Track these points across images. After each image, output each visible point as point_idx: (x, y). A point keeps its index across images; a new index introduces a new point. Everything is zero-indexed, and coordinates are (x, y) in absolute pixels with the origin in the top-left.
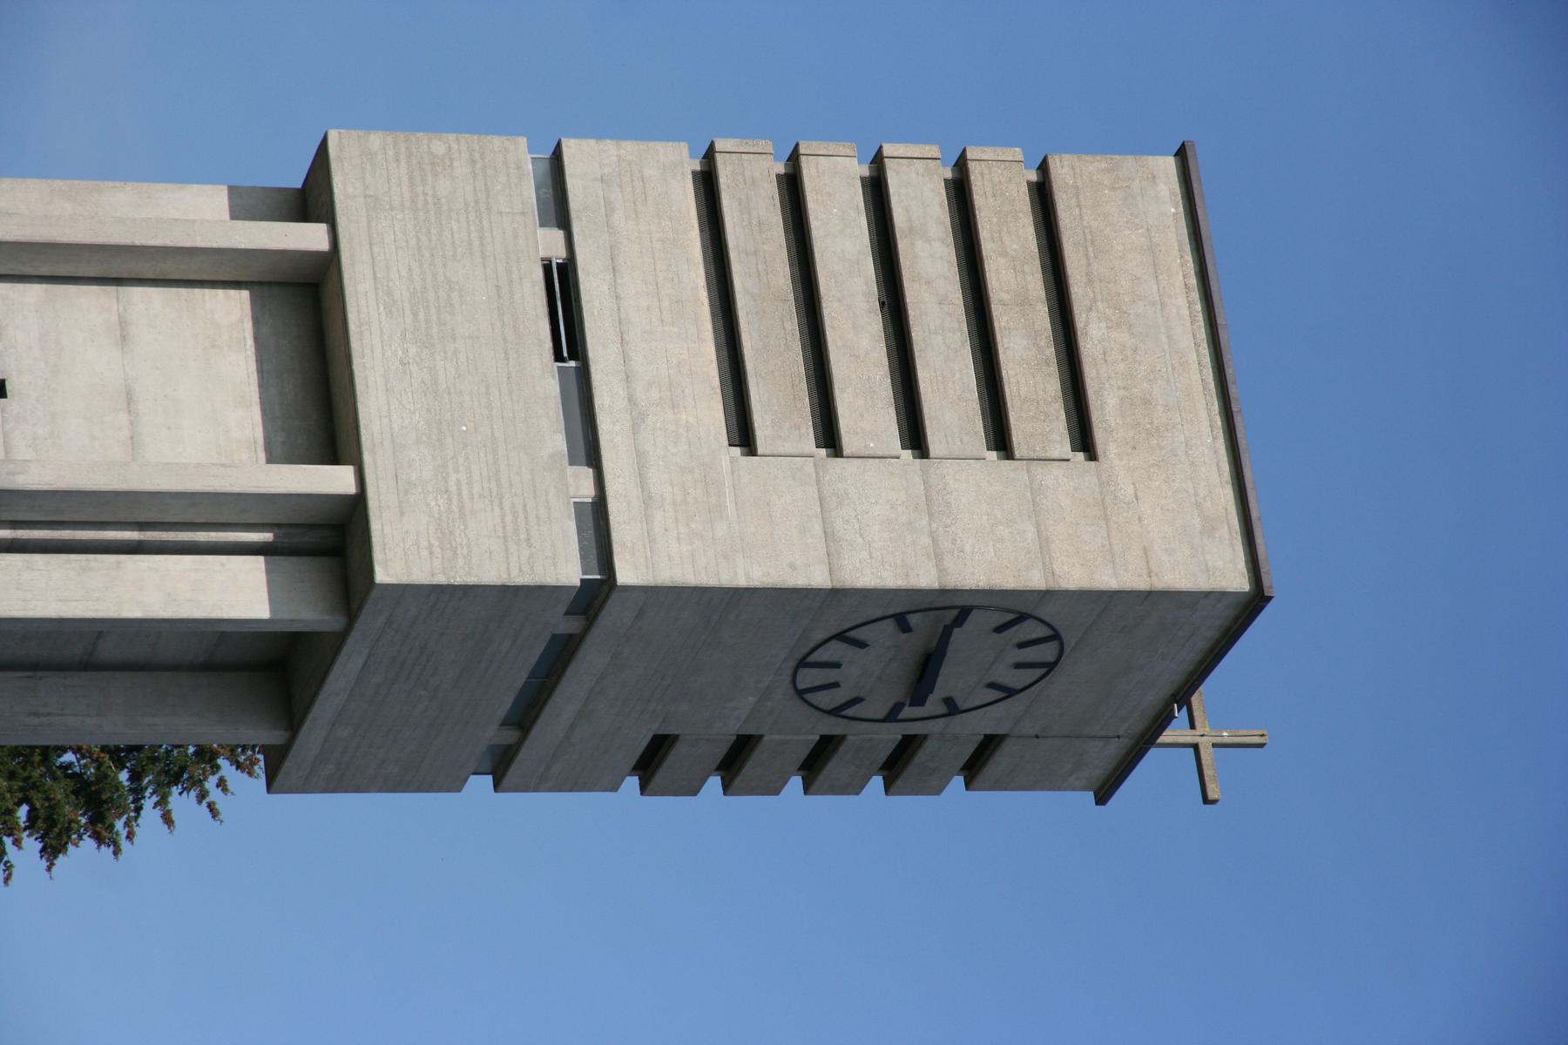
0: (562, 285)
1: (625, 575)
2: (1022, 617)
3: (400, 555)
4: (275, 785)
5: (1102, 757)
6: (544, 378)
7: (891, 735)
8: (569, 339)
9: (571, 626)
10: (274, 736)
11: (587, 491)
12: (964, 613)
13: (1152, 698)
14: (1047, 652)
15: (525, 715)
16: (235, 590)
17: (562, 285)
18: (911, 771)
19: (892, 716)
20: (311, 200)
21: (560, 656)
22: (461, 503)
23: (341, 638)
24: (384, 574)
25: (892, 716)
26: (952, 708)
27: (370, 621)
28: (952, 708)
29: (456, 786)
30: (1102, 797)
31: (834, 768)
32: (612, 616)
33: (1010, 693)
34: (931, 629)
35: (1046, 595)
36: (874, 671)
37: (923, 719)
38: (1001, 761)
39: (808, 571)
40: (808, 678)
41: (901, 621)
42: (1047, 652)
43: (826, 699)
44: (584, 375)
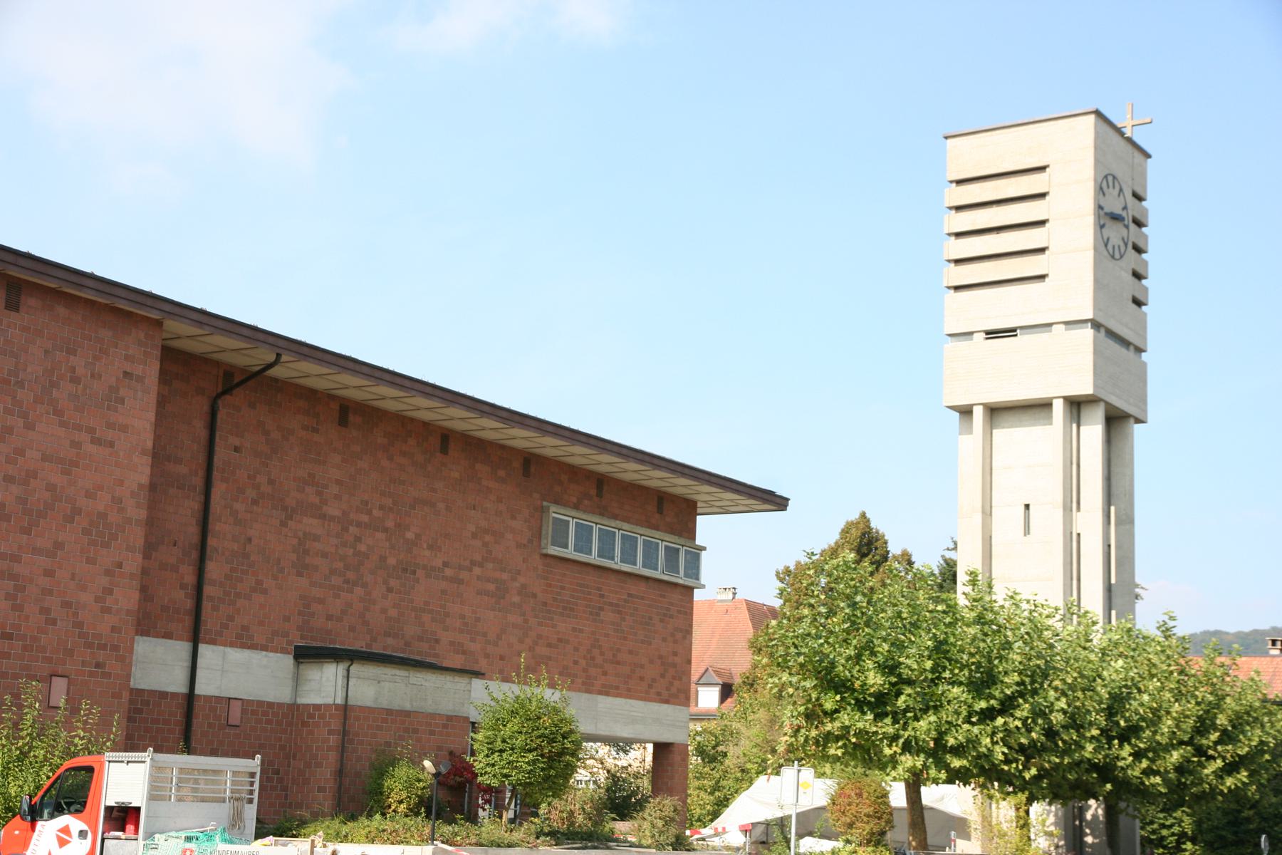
0: (992, 334)
1: (1091, 317)
2: (1101, 188)
3: (1085, 387)
4: (1140, 417)
5: (1138, 157)
6: (1022, 338)
7: (1132, 226)
8: (1010, 332)
9: (1103, 330)
10: (1132, 420)
11: (1063, 326)
12: (1100, 207)
13: (1123, 143)
14: (1110, 178)
17: (992, 334)
18: (1142, 220)
19: (1127, 227)
20: (966, 412)
21: (1111, 334)
22: (1070, 366)
23: (1107, 403)
24: (1090, 391)
25: (1127, 227)
26: (1125, 208)
28: (1125, 208)
30: (1149, 156)
32: (1101, 320)
33: (1121, 190)
34: (1107, 218)
35: (1095, 180)
36: (1115, 233)
38: (1139, 191)
40: (1117, 256)
41: (1102, 227)
42: (1110, 178)
43: (1123, 249)
44: (1021, 328)
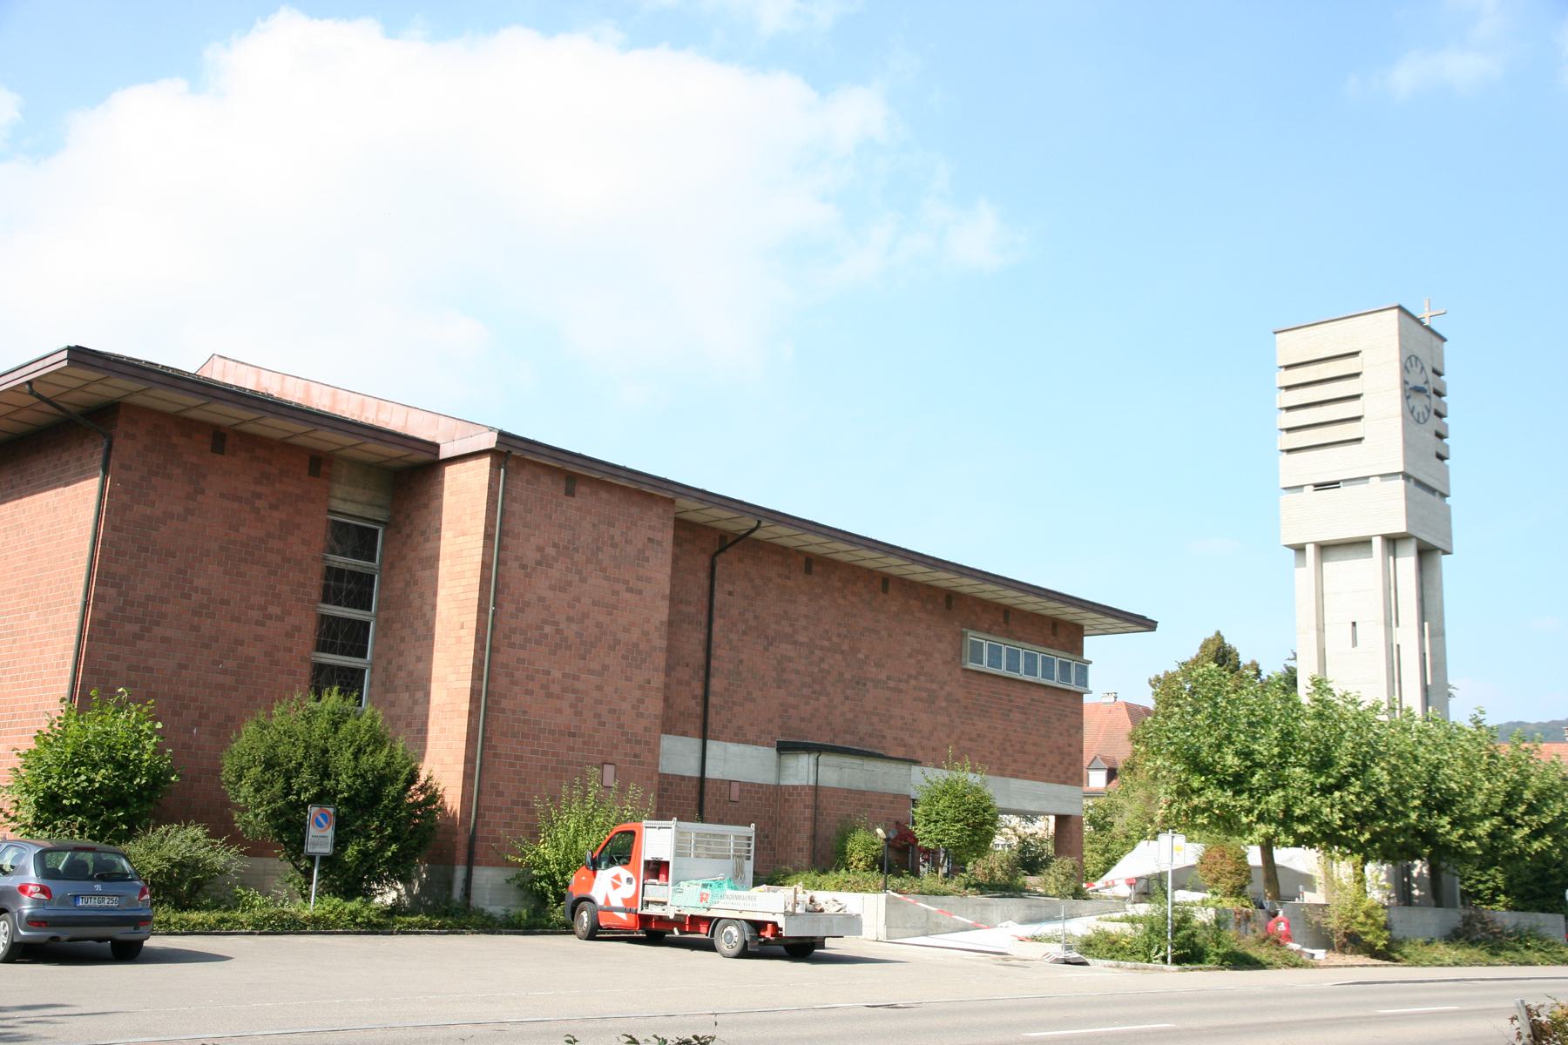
0: (1320, 486)
5: (1436, 341)
6: (1344, 490)
7: (1434, 397)
8: (1334, 484)
15: (1432, 490)
16: (1407, 563)
17: (1320, 486)
20: (1300, 549)
22: (1387, 510)
24: (1404, 530)
27: (1413, 532)
29: (1448, 507)
31: (1441, 411)
32: (1410, 472)
34: (1412, 391)
36: (1419, 402)
37: (1429, 389)
38: (1438, 368)
39: (1400, 419)
